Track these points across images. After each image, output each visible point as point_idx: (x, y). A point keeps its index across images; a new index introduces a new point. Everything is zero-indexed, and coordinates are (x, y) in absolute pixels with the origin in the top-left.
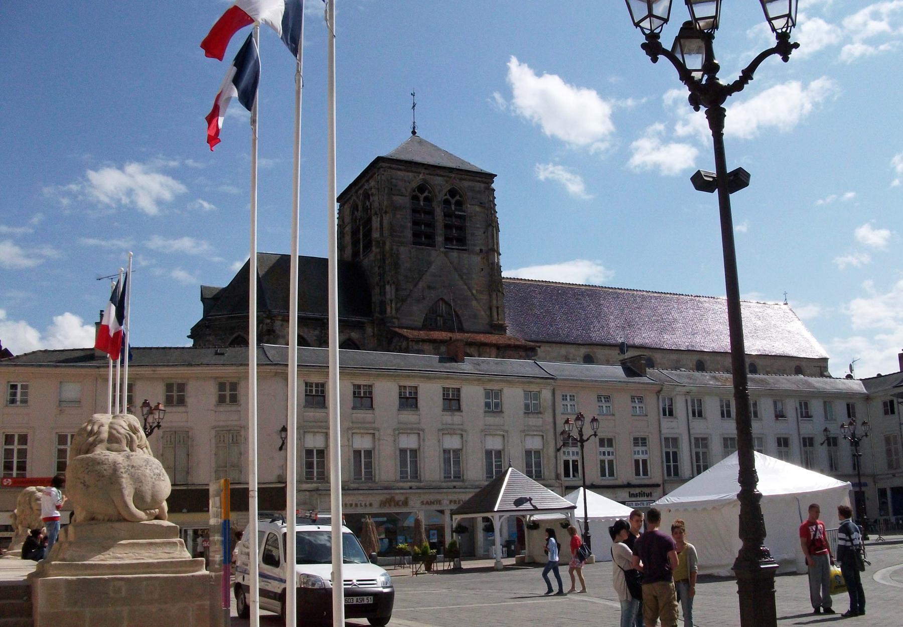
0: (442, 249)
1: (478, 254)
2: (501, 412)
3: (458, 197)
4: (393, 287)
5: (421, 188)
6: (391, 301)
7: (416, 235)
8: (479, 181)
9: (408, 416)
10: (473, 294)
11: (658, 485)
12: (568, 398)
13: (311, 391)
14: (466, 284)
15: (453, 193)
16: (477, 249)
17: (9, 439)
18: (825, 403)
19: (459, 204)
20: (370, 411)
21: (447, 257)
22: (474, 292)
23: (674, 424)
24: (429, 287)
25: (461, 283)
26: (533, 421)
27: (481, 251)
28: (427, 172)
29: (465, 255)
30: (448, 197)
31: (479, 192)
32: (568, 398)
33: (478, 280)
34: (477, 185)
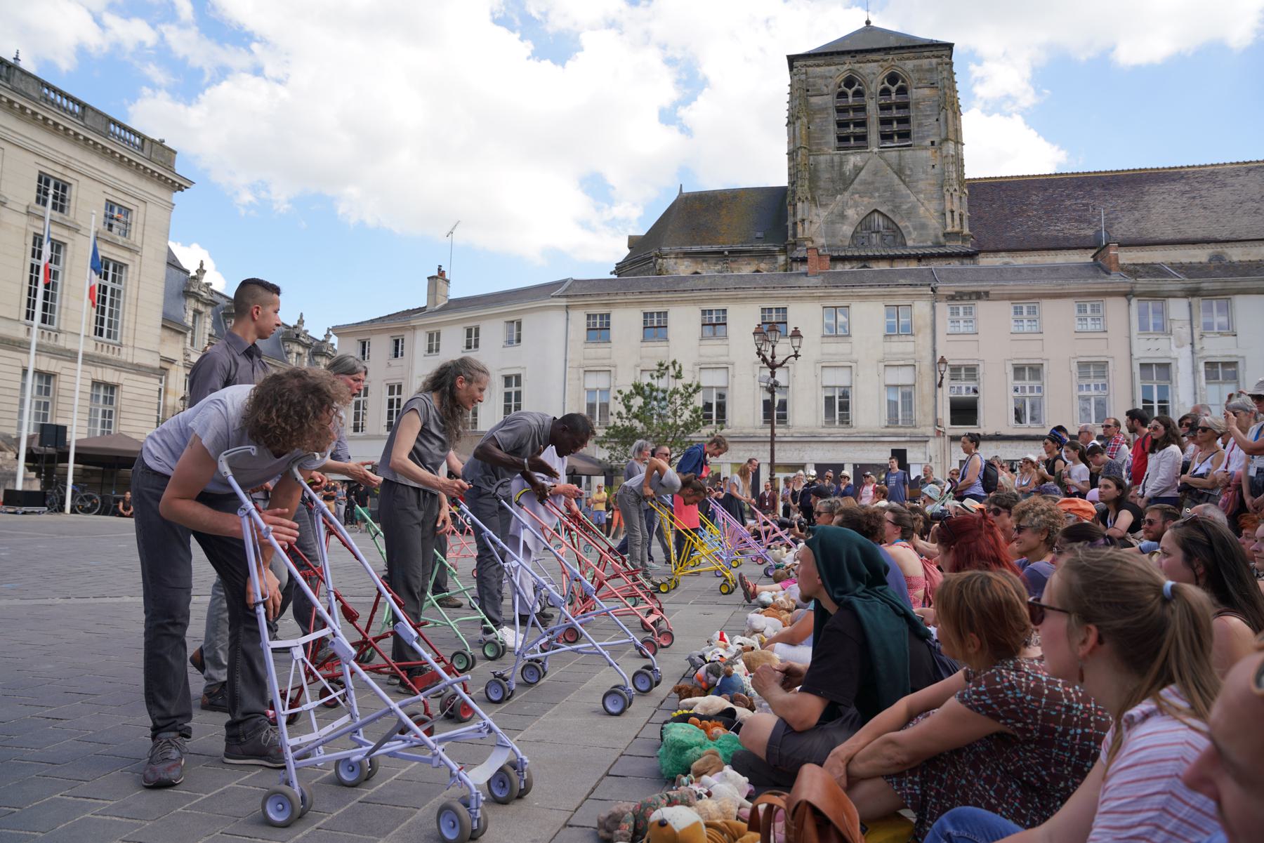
0: (876, 150)
1: (926, 148)
2: (849, 335)
3: (900, 83)
5: (849, 82)
12: (1089, 309)
13: (595, 324)
15: (893, 78)
16: (928, 142)
17: (391, 389)
19: (902, 91)
20: (664, 343)
26: (900, 347)
27: (933, 143)
29: (908, 154)
30: (887, 84)
31: (930, 70)
32: (1089, 309)
34: (925, 63)
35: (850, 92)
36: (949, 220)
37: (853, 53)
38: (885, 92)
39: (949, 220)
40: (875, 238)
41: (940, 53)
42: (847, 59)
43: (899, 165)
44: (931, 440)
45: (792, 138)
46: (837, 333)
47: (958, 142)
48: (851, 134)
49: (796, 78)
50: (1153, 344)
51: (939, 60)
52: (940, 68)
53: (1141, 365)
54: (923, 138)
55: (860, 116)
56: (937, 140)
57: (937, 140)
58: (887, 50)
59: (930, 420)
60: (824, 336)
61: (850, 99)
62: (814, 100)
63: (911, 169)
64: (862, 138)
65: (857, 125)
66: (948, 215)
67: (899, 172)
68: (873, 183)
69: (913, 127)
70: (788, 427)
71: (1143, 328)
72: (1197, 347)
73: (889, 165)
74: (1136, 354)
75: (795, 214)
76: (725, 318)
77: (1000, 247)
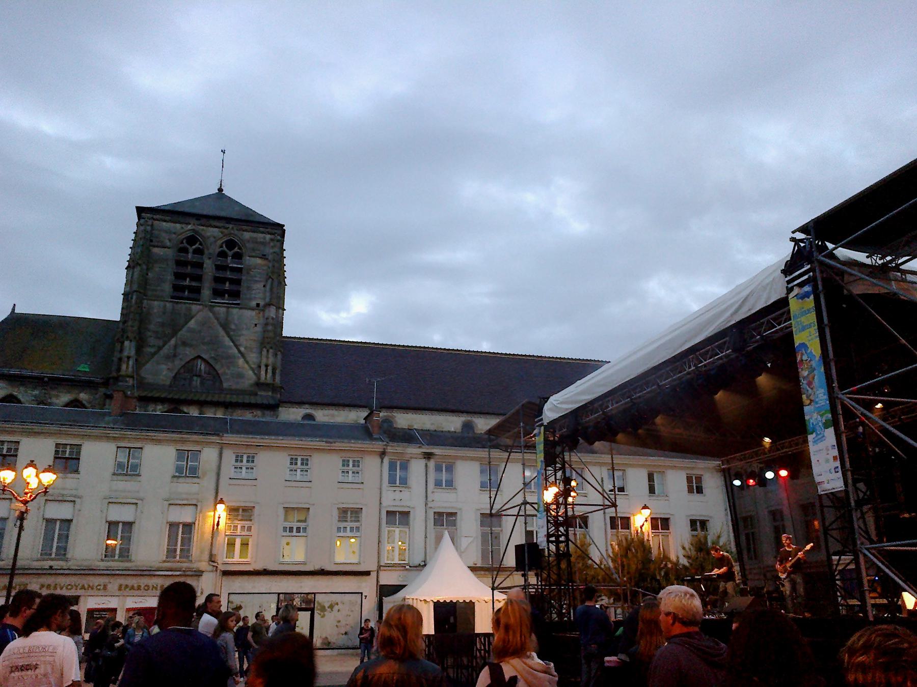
1: (253, 309)
3: (236, 249)
4: (133, 344)
5: (192, 240)
6: (129, 358)
7: (176, 288)
8: (263, 233)
9: (124, 485)
10: (240, 351)
11: (368, 573)
12: (299, 462)
14: (233, 342)
15: (231, 244)
16: (254, 303)
18: (651, 477)
19: (238, 256)
21: (211, 311)
22: (242, 349)
23: (405, 495)
24: (184, 344)
25: (227, 339)
27: (258, 305)
28: (198, 222)
31: (264, 244)
32: (299, 462)
33: (249, 336)
35: (191, 250)
36: (263, 373)
37: (198, 217)
38: (222, 254)
39: (263, 373)
40: (197, 381)
41: (274, 231)
42: (193, 221)
43: (227, 319)
44: (205, 575)
45: (129, 282)
46: (128, 470)
47: (281, 307)
48: (186, 285)
49: (142, 228)
50: (398, 495)
51: (272, 237)
52: (272, 244)
53: (387, 512)
54: (250, 299)
55: (197, 271)
56: (262, 303)
57: (262, 303)
58: (228, 220)
59: (206, 556)
60: (114, 474)
61: (190, 256)
62: (156, 250)
63: (235, 325)
64: (197, 291)
65: (192, 279)
66: (263, 368)
67: (225, 326)
68: (200, 332)
69: (243, 289)
70: (130, 561)
71: (392, 481)
72: (429, 499)
73: (217, 319)
74: (384, 503)
75: (121, 351)
76: (17, 450)
77: (305, 400)
